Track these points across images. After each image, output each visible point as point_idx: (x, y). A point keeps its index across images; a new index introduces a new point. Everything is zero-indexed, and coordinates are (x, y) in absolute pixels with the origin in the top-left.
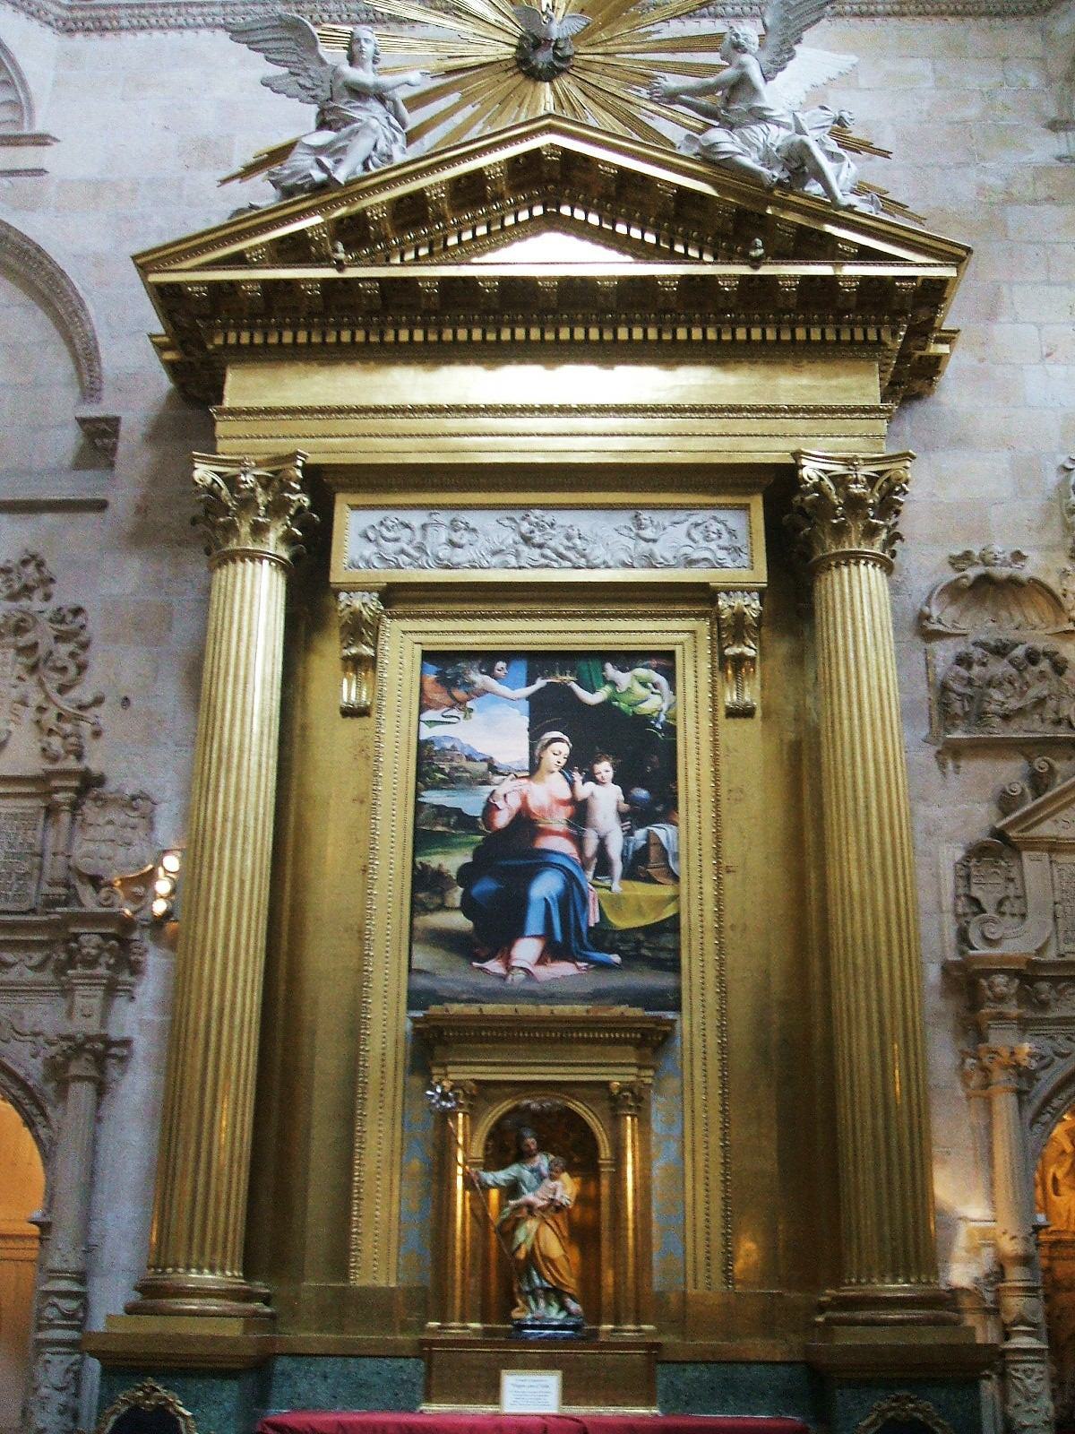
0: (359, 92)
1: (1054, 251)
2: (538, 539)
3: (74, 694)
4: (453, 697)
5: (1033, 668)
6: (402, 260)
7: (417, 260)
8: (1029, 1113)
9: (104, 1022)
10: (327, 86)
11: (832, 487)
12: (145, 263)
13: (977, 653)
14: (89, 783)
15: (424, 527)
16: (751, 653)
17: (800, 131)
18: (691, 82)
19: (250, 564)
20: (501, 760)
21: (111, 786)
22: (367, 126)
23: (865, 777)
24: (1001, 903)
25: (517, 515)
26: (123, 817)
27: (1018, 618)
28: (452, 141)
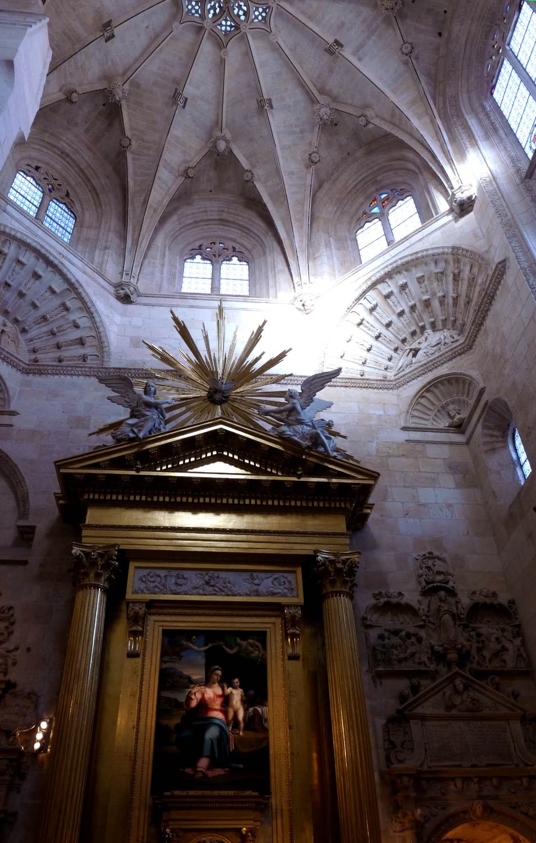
0: (148, 405)
1: (406, 474)
2: (212, 583)
5: (408, 641)
6: (161, 469)
7: (167, 470)
10: (136, 402)
12: (59, 465)
13: (386, 634)
15: (166, 576)
16: (298, 632)
17: (314, 427)
18: (274, 408)
20: (194, 677)
21: (18, 689)
22: (152, 418)
24: (403, 743)
25: (204, 573)
27: (402, 620)
28: (182, 425)
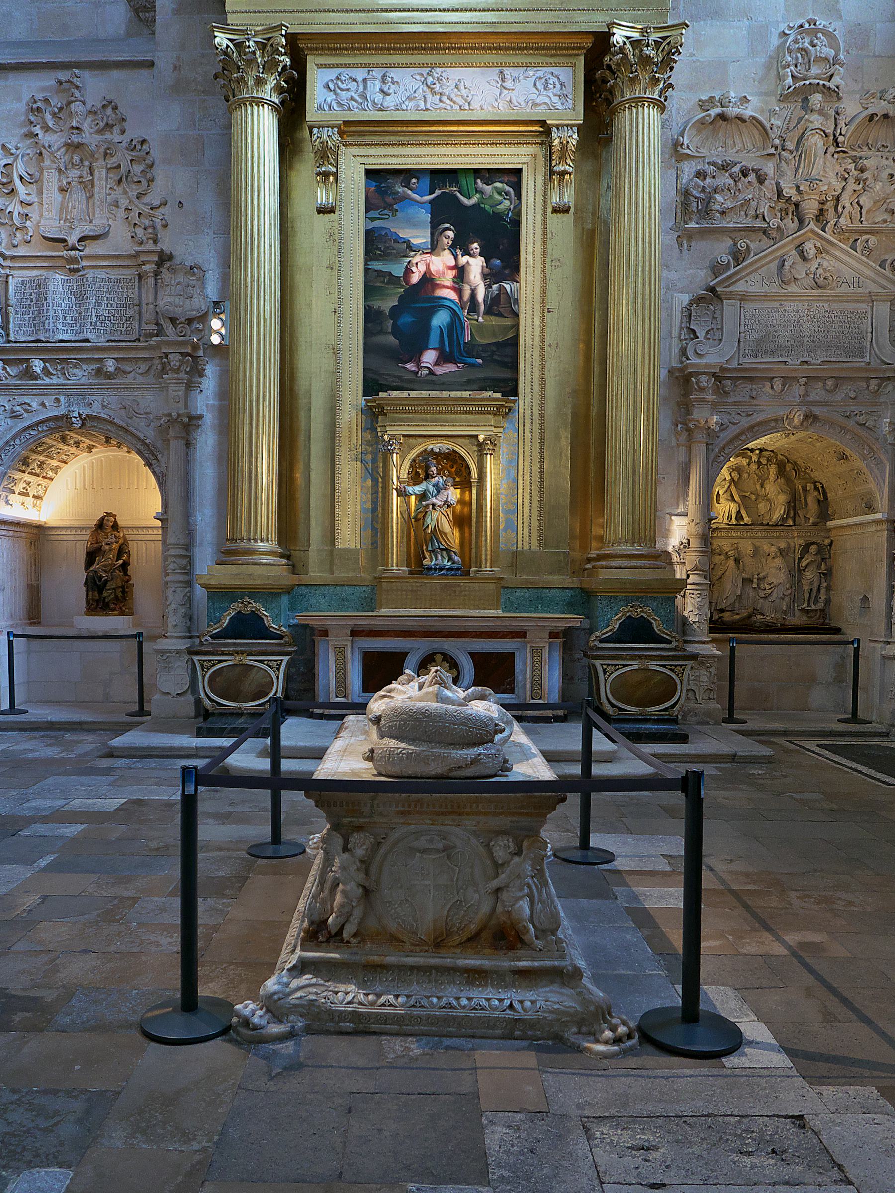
3: (146, 199)
4: (385, 202)
8: (712, 456)
9: (186, 406)
11: (631, 50)
14: (164, 258)
15: (365, 80)
16: (571, 170)
19: (256, 108)
20: (415, 241)
21: (177, 261)
23: (637, 251)
25: (425, 71)
26: (186, 280)
